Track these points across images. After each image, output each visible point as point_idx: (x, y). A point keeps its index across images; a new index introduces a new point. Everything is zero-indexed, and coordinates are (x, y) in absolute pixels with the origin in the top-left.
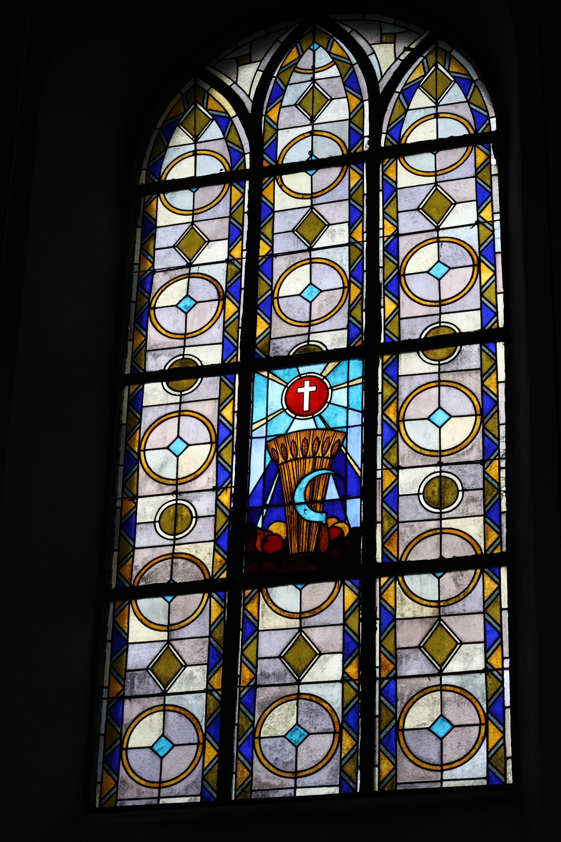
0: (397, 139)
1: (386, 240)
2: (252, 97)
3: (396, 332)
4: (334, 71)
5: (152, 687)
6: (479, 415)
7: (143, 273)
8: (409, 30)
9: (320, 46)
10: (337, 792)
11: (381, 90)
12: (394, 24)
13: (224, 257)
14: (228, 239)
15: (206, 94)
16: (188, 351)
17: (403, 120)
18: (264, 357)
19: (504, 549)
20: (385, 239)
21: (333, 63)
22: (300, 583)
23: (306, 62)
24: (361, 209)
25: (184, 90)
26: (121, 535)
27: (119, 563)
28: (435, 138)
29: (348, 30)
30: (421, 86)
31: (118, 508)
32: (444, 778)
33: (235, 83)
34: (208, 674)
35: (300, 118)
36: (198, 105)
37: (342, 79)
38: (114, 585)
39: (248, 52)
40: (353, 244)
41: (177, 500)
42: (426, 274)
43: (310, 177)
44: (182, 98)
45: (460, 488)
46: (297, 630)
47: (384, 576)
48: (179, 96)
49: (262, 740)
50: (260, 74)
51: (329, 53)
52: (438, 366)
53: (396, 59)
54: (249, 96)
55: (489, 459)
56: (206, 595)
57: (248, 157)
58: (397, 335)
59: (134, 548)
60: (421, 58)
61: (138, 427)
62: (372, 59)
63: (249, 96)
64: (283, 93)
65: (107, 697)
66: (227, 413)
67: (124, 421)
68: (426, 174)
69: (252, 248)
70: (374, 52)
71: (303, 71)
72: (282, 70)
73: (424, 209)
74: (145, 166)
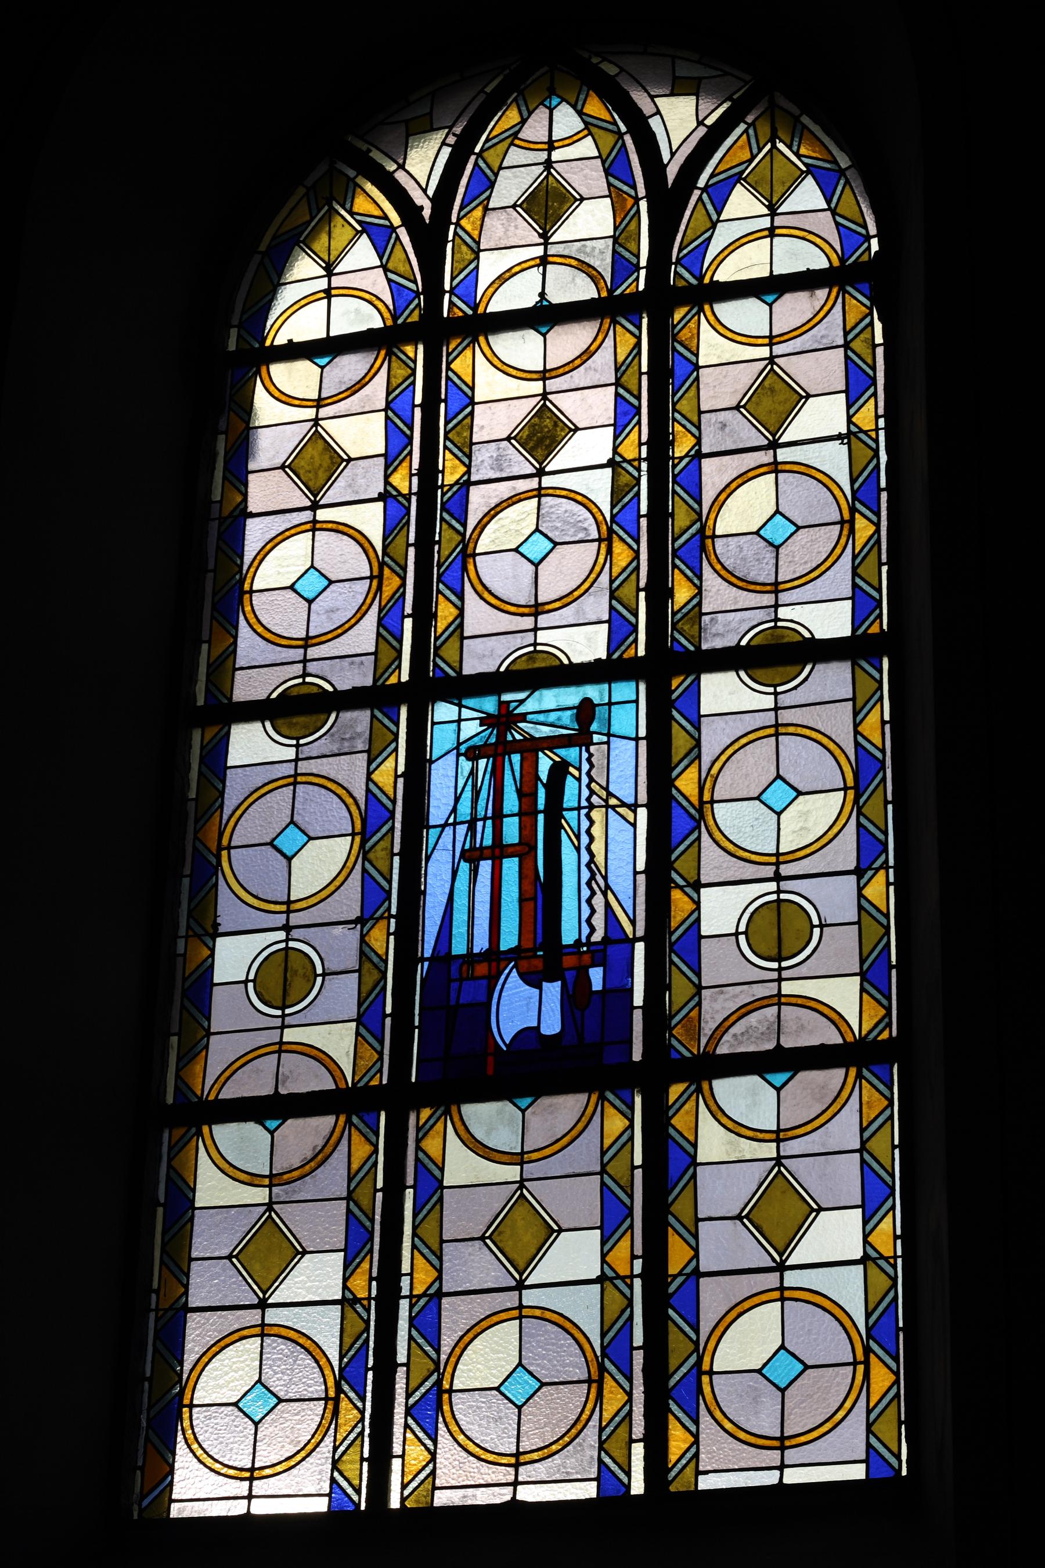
0: (697, 273)
1: (870, 437)
2: (431, 192)
4: (587, 147)
5: (494, 1273)
6: (851, 788)
7: (448, 487)
8: (726, 74)
9: (563, 100)
10: (593, 1494)
11: (670, 182)
12: (699, 62)
13: (606, 455)
14: (846, 391)
15: (351, 185)
16: (543, 637)
17: (710, 239)
18: (692, 648)
19: (894, 1033)
20: (445, 489)
21: (586, 132)
23: (535, 130)
24: (635, 402)
25: (309, 182)
26: (183, 1007)
27: (179, 1059)
28: (324, 335)
29: (612, 70)
30: (745, 179)
31: (180, 955)
32: (786, 1462)
33: (402, 167)
34: (345, 1268)
35: (525, 230)
36: (334, 204)
37: (603, 162)
38: (170, 1100)
39: (428, 110)
40: (855, 434)
42: (513, 553)
43: (768, 307)
44: (307, 194)
45: (816, 922)
46: (263, 1209)
48: (301, 191)
49: (195, 1410)
50: (446, 151)
51: (580, 113)
52: (773, 697)
53: (700, 123)
54: (425, 191)
55: (371, 918)
56: (594, 1097)
57: (643, 273)
58: (456, 665)
59: (209, 1034)
60: (742, 127)
61: (217, 804)
62: (655, 123)
63: (425, 191)
64: (492, 185)
65: (408, 1293)
66: (871, 725)
67: (193, 795)
68: (750, 340)
69: (429, 471)
70: (658, 112)
71: (529, 146)
72: (488, 145)
74: (235, 321)
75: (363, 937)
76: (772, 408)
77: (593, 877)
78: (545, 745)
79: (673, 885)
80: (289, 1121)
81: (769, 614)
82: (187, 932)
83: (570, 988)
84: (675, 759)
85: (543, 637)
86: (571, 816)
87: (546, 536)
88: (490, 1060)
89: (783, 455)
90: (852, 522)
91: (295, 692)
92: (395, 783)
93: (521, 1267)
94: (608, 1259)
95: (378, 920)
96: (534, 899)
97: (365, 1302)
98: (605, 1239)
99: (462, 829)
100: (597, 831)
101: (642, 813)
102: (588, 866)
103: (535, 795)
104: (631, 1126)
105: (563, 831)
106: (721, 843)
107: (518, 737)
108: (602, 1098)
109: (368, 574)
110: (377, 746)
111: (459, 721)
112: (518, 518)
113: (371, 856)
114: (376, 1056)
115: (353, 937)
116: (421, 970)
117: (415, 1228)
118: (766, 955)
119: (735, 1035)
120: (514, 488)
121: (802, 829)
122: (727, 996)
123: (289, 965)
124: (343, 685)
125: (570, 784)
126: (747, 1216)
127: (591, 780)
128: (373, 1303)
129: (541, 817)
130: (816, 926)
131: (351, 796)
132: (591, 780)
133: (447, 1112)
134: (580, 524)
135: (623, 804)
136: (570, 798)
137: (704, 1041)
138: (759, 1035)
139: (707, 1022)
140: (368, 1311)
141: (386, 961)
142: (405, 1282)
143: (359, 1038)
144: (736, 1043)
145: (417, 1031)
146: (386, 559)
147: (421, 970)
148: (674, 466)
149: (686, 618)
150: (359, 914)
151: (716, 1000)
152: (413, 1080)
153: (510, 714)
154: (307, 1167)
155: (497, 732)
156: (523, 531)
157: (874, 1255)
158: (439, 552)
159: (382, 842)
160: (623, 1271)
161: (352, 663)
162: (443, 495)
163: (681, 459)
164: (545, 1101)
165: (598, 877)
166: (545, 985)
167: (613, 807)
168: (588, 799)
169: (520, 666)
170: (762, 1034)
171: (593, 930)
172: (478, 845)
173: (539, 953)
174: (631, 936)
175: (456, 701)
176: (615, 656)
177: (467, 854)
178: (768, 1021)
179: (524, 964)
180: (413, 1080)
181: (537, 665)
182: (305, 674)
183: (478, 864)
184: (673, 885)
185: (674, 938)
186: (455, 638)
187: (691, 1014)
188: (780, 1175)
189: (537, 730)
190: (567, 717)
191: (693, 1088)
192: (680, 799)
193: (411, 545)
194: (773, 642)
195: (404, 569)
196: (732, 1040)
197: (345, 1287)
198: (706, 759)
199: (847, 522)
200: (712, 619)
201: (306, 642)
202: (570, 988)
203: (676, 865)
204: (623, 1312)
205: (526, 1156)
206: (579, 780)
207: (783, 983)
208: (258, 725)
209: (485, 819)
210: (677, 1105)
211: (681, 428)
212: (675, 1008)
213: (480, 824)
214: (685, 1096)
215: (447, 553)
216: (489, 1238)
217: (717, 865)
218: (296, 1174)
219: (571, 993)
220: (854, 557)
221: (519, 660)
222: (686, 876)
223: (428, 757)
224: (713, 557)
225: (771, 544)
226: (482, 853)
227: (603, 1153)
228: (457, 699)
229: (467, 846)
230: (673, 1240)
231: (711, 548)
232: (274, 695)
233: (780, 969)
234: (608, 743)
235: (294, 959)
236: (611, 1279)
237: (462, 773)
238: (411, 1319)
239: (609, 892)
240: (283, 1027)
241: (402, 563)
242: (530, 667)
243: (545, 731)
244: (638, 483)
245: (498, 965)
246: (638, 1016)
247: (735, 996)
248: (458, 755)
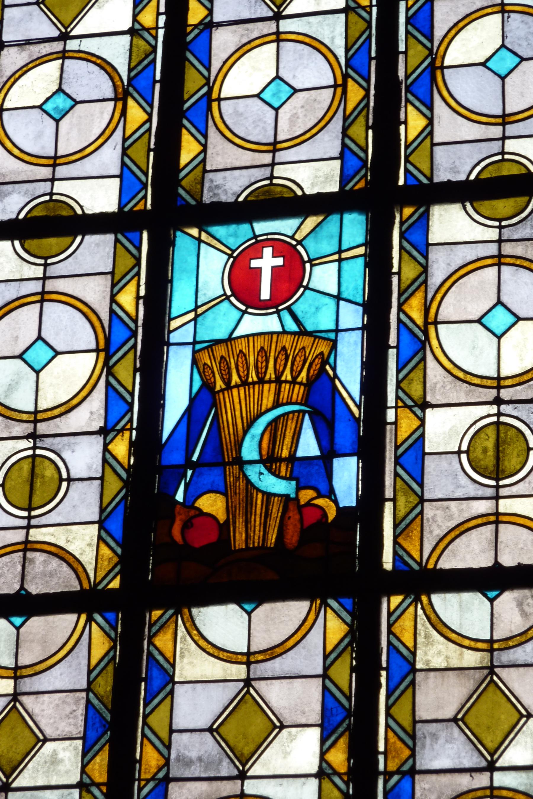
16: (59, 187)
18: (193, 203)
41: (34, 448)
46: (242, 684)
58: (427, 172)
82: (397, 403)
85: (511, 145)
90: (344, 86)
108: (90, 620)
109: (332, 82)
146: (350, 71)
150: (102, 424)
164: (265, 608)
193: (158, 81)
199: (340, 85)
201: (275, 147)
207: (501, 501)
208: (8, 243)
220: (345, 119)
227: (90, 672)
233: (29, 518)
240: (28, 527)
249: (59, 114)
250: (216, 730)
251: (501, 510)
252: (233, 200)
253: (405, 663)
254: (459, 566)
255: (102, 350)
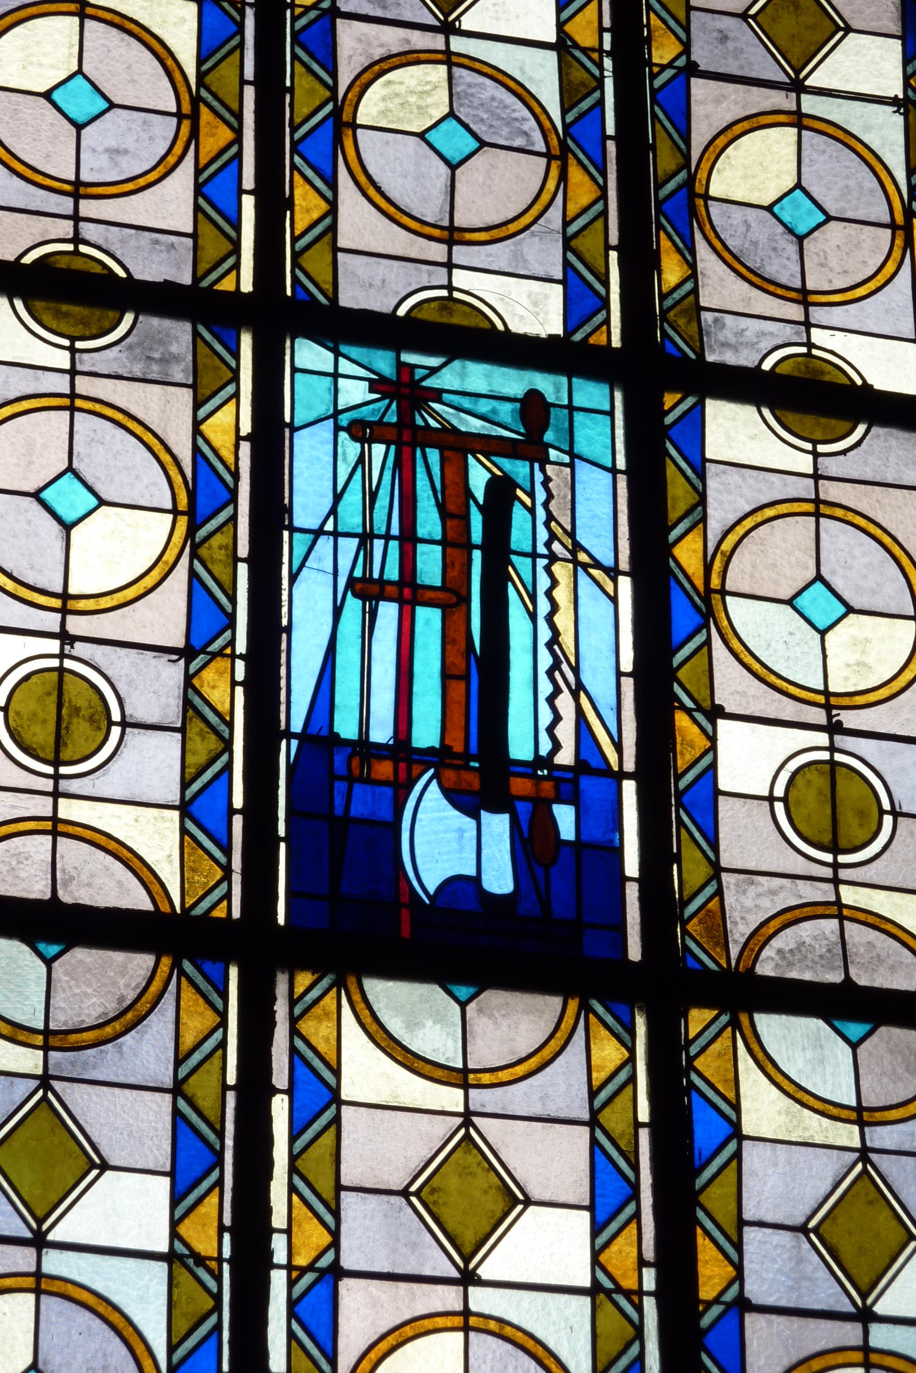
3: (325, 277)
22: (51, 940)
41: (62, 656)
46: (34, 1083)
47: (304, 968)
73: (833, 28)
75: (188, 679)
76: (795, 32)
77: (556, 666)
78: (478, 447)
79: (676, 704)
80: (883, 1030)
81: (797, 333)
83: (525, 826)
84: (673, 516)
85: (461, 278)
86: (523, 564)
87: (466, 127)
88: (405, 914)
89: (458, 44)
90: (195, 118)
91: (63, 263)
92: (237, 447)
93: (468, 1249)
94: (603, 1258)
95: (214, 655)
96: (466, 678)
97: (213, 1265)
98: (597, 1228)
99: (349, 546)
100: (562, 595)
101: (625, 585)
102: (549, 645)
103: (466, 518)
104: (631, 1060)
105: (510, 584)
106: (742, 656)
107: (433, 423)
110: (207, 382)
111: (336, 375)
112: (420, 88)
113: (203, 552)
114: (219, 874)
115: (174, 673)
116: (286, 752)
117: (293, 1159)
118: (814, 839)
119: (780, 951)
120: (408, 41)
121: (858, 664)
122: (760, 890)
123: (66, 697)
124: (142, 273)
125: (519, 516)
126: (816, 1230)
127: (550, 517)
128: (226, 1267)
129: (477, 555)
130: (116, 724)
131: (168, 450)
132: (550, 517)
133: (340, 984)
134: (517, 124)
135: (598, 565)
136: (519, 537)
137: (734, 951)
138: (817, 959)
139: (736, 923)
140: (219, 1279)
141: (230, 725)
142: (279, 1244)
143: (186, 838)
144: (784, 963)
145: (283, 846)
146: (204, 93)
147: (286, 752)
148: (653, 76)
149: (678, 308)
151: (744, 892)
152: (281, 920)
153: (415, 384)
154: (108, 1030)
155: (398, 407)
156: (430, 111)
157: (608, 1284)
158: (292, 105)
159: (218, 536)
160: (629, 1283)
161: (157, 242)
162: (294, 19)
163: (663, 68)
165: (565, 667)
166: (485, 816)
167: (585, 566)
168: (548, 545)
169: (429, 315)
170: (821, 957)
171: (557, 746)
172: (376, 575)
173: (472, 764)
174: (616, 769)
175: (331, 345)
176: (578, 337)
177: (359, 586)
178: (827, 939)
179: (450, 775)
180: (281, 920)
181: (456, 320)
182: (77, 240)
183: (377, 605)
184: (676, 704)
185: (682, 784)
186: (323, 246)
187: (710, 905)
188: (865, 1176)
189: (467, 423)
190: (506, 411)
191: (724, 1019)
192: (681, 577)
194: (807, 376)
195: (239, 117)
196: (777, 958)
197: (174, 1234)
198: (715, 527)
200: (716, 320)
202: (525, 826)
203: (682, 674)
204: (628, 1345)
205: (471, 1076)
206: (532, 511)
209: (387, 537)
210: (702, 1041)
211: (659, 23)
212: (687, 894)
213: (378, 544)
214: (714, 1029)
215: (306, 111)
216: (417, 1194)
217: (740, 689)
218: (87, 1036)
219: (526, 835)
221: (426, 305)
222: (696, 695)
223: (287, 419)
224: (708, 227)
225: (791, 231)
226: (382, 590)
228: (332, 341)
229: (358, 573)
230: (706, 1251)
231: (704, 213)
232: (28, 260)
234: (571, 465)
235: (72, 687)
236: (608, 1293)
237: (345, 459)
238: (292, 1304)
239: (582, 694)
240: (56, 794)
241: (235, 106)
242: (444, 320)
243: (474, 425)
244: (601, 86)
245: (409, 770)
246: (632, 892)
247: (773, 893)
248: (337, 429)
249: (794, 201)
250: (93, 1165)
251: (62, 815)
252: (12, 259)
253: (325, 1091)
254: (895, 986)
255: (183, 513)
